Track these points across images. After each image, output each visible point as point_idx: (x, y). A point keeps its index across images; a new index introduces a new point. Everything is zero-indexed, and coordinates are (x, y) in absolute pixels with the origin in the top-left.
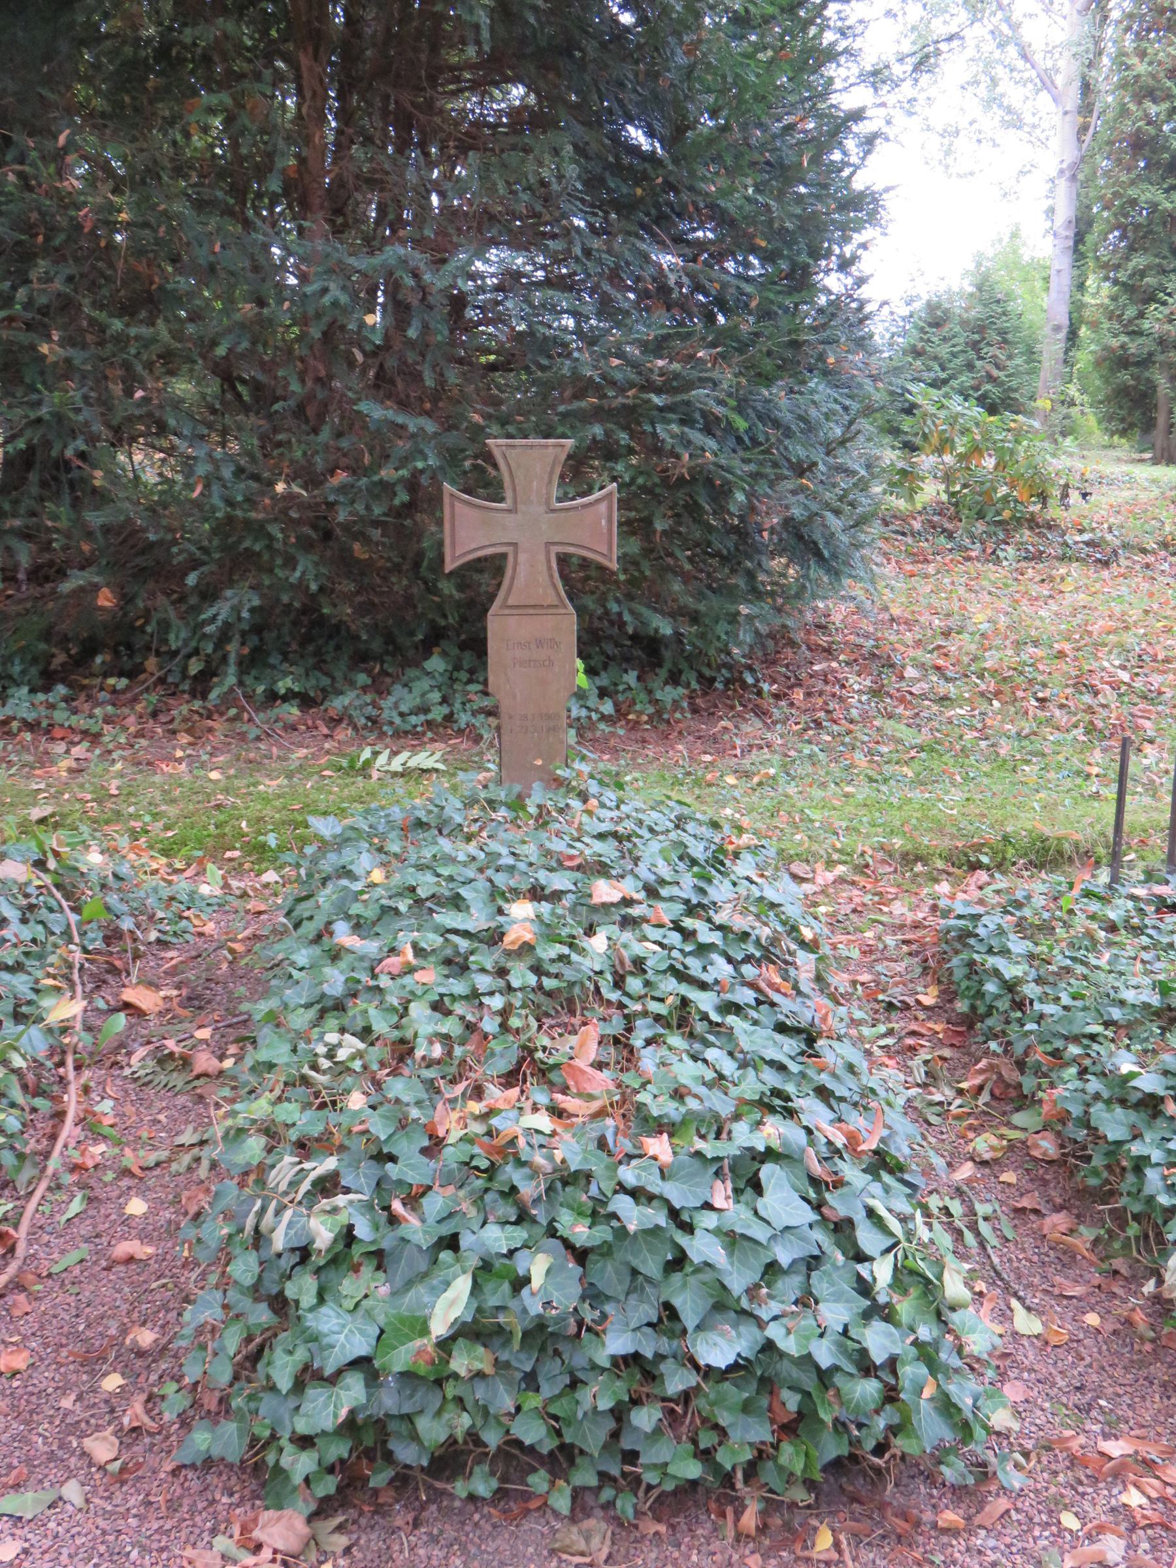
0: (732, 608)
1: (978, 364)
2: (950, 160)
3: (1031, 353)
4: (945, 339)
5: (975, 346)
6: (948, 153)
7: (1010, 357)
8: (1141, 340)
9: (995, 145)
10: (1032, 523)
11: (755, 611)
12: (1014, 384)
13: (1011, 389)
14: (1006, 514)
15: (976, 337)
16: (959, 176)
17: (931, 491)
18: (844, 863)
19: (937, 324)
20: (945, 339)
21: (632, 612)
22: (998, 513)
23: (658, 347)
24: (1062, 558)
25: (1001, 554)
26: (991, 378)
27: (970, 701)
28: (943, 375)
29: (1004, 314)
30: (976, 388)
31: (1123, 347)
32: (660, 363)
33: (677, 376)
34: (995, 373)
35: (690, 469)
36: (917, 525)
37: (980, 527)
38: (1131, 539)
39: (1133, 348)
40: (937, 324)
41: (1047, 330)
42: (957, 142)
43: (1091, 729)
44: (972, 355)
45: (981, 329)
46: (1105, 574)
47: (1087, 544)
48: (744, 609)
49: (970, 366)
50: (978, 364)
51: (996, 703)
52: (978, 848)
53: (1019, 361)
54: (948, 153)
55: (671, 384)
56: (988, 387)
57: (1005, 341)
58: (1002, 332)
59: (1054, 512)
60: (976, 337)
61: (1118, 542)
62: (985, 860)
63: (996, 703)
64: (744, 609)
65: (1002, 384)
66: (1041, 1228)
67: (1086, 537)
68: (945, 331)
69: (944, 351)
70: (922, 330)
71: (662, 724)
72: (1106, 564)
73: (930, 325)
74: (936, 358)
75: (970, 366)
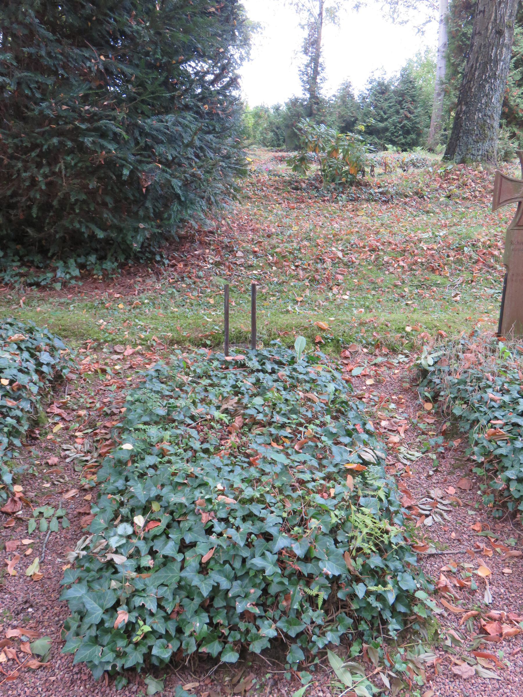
0: (136, 225)
1: (401, 111)
2: (395, 16)
3: (426, 106)
4: (386, 100)
5: (400, 103)
6: (394, 12)
7: (416, 108)
9: (415, 8)
10: (359, 184)
11: (147, 226)
12: (417, 120)
13: (416, 123)
14: (344, 180)
15: (401, 99)
16: (401, 23)
17: (314, 168)
18: (141, 344)
19: (383, 93)
20: (386, 100)
21: (87, 227)
22: (340, 180)
23: (85, 99)
24: (368, 200)
25: (339, 198)
26: (407, 118)
27: (262, 268)
28: (385, 117)
29: (413, 87)
30: (400, 123)
32: (87, 108)
33: (95, 114)
34: (409, 115)
35: (105, 160)
36: (304, 185)
37: (332, 186)
38: (400, 191)
40: (383, 93)
41: (435, 95)
42: (398, 7)
43: (313, 280)
44: (399, 107)
45: (403, 95)
46: (385, 207)
47: (381, 193)
48: (142, 226)
49: (398, 112)
50: (401, 111)
51: (274, 268)
52: (206, 337)
53: (419, 109)
54: (394, 12)
55: (93, 118)
56: (405, 122)
57: (414, 101)
58: (412, 96)
59: (367, 178)
60: (401, 99)
61: (394, 192)
62: (208, 342)
63: (274, 268)
64: (142, 226)
65: (412, 120)
66: (79, 523)
67: (381, 190)
68: (386, 96)
69: (386, 105)
70: (375, 95)
71: (108, 280)
72: (386, 202)
73: (379, 93)
74: (382, 109)
75: (398, 112)
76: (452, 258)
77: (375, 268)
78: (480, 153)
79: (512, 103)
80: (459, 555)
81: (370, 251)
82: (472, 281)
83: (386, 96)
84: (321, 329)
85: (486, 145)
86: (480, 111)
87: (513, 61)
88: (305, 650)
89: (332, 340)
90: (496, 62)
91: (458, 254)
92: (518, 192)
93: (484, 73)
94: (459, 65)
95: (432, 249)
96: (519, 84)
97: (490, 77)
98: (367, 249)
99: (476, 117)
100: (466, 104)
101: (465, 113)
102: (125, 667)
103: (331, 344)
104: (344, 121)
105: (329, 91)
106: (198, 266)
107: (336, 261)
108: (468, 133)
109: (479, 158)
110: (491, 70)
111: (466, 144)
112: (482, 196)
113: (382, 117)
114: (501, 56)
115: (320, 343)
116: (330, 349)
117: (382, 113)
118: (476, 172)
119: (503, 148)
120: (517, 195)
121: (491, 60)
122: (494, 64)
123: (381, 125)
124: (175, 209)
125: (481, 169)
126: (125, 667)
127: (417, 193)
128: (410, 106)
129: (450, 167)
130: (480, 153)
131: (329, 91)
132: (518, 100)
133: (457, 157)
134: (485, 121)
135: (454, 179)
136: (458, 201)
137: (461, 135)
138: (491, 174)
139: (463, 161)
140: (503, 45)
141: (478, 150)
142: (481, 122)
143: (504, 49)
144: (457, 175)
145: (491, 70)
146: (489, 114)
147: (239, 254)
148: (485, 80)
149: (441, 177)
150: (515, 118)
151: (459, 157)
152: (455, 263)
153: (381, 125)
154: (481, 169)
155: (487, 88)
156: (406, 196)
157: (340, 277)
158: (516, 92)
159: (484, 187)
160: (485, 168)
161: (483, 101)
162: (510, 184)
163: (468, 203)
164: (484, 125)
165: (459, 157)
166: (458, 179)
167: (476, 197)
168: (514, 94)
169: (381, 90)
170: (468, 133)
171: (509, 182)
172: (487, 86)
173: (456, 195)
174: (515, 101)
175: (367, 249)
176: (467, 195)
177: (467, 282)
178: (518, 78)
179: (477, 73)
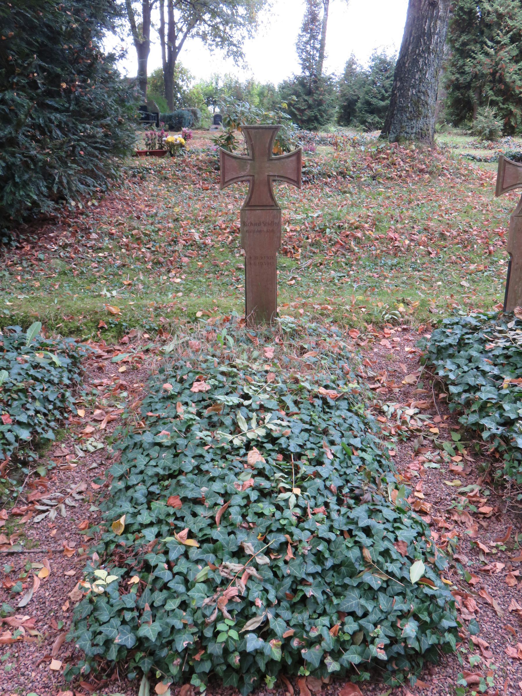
8: (465, 77)
31: (457, 79)
39: (461, 80)
76: (310, 240)
77: (227, 251)
78: (414, 131)
79: (508, 80)
80: (41, 554)
81: (229, 232)
82: (321, 264)
84: (111, 314)
85: (420, 123)
86: (414, 87)
87: (509, 35)
89: (116, 325)
90: (430, 36)
91: (319, 236)
92: (244, 170)
94: (456, 40)
95: (295, 231)
96: (516, 60)
97: (423, 51)
98: (228, 230)
99: (410, 93)
100: (401, 80)
101: (400, 89)
103: (114, 329)
104: (347, 99)
105: (333, 68)
106: (46, 248)
107: (191, 244)
108: (402, 110)
110: (425, 44)
111: (400, 122)
112: (408, 176)
113: (383, 95)
114: (435, 29)
115: (102, 328)
116: (110, 334)
117: (383, 91)
118: (408, 151)
119: (488, 127)
120: (243, 174)
121: (424, 34)
122: (428, 38)
123: (382, 103)
124: (8, 190)
125: (413, 147)
127: (341, 173)
129: (383, 145)
130: (414, 131)
131: (333, 68)
132: (515, 77)
133: (392, 136)
134: (419, 98)
135: (384, 158)
136: (381, 181)
137: (395, 112)
138: (422, 152)
139: (397, 140)
140: (438, 17)
141: (412, 128)
142: (415, 99)
143: (439, 22)
144: (387, 154)
146: (424, 90)
147: (94, 236)
148: (419, 55)
149: (371, 157)
150: (512, 95)
151: (393, 136)
152: (312, 245)
153: (382, 103)
154: (413, 147)
155: (421, 63)
156: (329, 177)
157: (185, 259)
158: (513, 68)
159: (412, 166)
160: (417, 147)
161: (417, 77)
162: (235, 163)
163: (390, 184)
164: (418, 102)
165: (393, 136)
166: (388, 159)
167: (400, 176)
168: (511, 70)
169: (381, 66)
170: (402, 110)
171: (234, 160)
172: (421, 60)
173: (380, 175)
174: (511, 77)
175: (228, 230)
176: (393, 175)
177: (316, 265)
178: (515, 53)
179: (411, 48)
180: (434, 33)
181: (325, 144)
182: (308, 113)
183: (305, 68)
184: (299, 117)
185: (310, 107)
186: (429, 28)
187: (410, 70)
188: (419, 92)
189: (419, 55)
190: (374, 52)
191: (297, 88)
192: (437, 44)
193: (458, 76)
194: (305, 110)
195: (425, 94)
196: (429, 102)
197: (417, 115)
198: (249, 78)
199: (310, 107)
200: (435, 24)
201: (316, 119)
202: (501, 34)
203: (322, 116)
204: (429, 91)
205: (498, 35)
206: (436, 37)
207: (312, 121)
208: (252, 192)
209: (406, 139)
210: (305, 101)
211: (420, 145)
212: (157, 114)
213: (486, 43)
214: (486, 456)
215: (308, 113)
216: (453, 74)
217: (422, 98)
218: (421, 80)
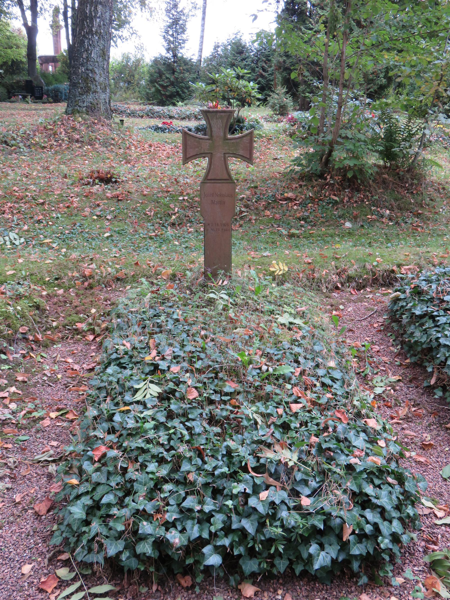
12: (271, 78)
26: (262, 76)
31: (284, 61)
34: (264, 73)
56: (260, 79)
65: (266, 78)
73: (238, 53)
78: (85, 105)
83: (243, 56)
85: (90, 98)
86: (82, 65)
88: (273, 565)
90: (92, 19)
93: (83, 29)
99: (80, 71)
102: (191, 539)
109: (84, 109)
110: (88, 26)
121: (86, 17)
126: (191, 539)
128: (264, 65)
134: (88, 75)
142: (84, 76)
143: (100, 7)
145: (88, 26)
146: (90, 68)
148: (84, 36)
164: (87, 78)
172: (86, 41)
180: (95, 16)
181: (134, 116)
182: (171, 89)
183: (168, 50)
184: (163, 93)
185: (172, 84)
186: (90, 11)
187: (78, 50)
188: (87, 70)
189: (84, 36)
190: (234, 36)
191: (160, 67)
192: (99, 26)
193: (285, 58)
194: (167, 86)
195: (92, 71)
196: (97, 78)
197: (88, 90)
198: (139, 56)
199: (172, 84)
200: (96, 8)
201: (178, 94)
202: (313, 22)
203: (184, 92)
204: (96, 70)
205: (310, 23)
206: (98, 20)
207: (175, 96)
208: (236, 155)
209: (79, 112)
210: (167, 78)
211: (87, 117)
212: (42, 88)
213: (301, 30)
214: (418, 358)
215: (171, 89)
216: (281, 56)
217: (90, 75)
218: (88, 59)
